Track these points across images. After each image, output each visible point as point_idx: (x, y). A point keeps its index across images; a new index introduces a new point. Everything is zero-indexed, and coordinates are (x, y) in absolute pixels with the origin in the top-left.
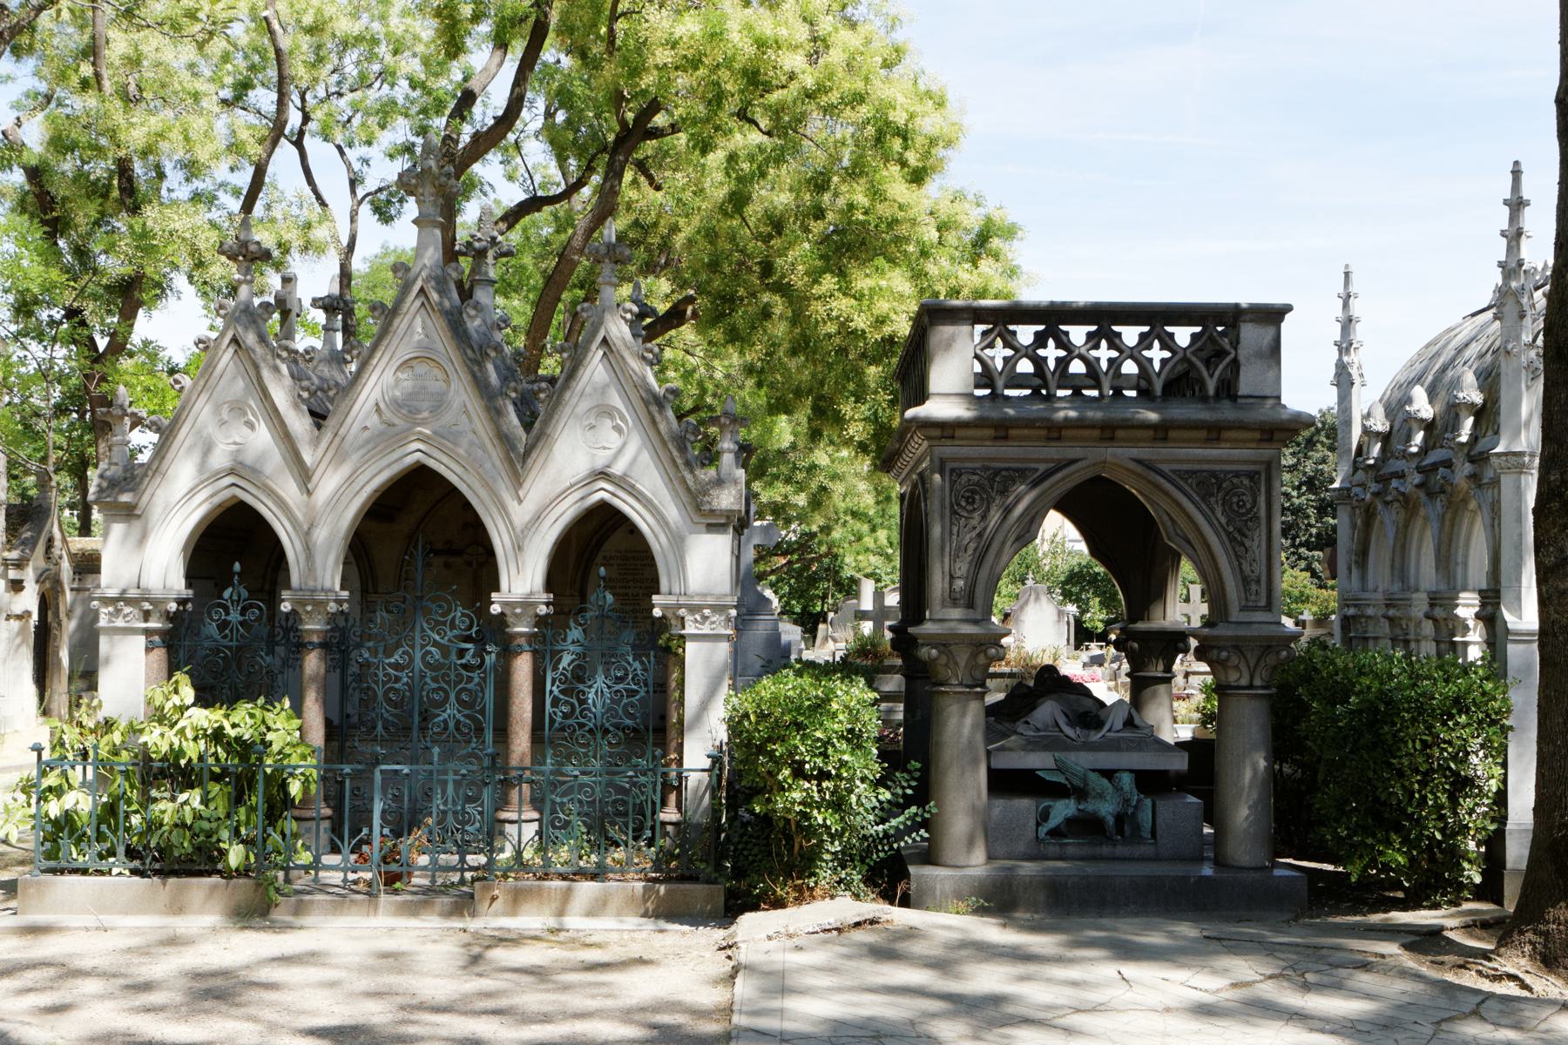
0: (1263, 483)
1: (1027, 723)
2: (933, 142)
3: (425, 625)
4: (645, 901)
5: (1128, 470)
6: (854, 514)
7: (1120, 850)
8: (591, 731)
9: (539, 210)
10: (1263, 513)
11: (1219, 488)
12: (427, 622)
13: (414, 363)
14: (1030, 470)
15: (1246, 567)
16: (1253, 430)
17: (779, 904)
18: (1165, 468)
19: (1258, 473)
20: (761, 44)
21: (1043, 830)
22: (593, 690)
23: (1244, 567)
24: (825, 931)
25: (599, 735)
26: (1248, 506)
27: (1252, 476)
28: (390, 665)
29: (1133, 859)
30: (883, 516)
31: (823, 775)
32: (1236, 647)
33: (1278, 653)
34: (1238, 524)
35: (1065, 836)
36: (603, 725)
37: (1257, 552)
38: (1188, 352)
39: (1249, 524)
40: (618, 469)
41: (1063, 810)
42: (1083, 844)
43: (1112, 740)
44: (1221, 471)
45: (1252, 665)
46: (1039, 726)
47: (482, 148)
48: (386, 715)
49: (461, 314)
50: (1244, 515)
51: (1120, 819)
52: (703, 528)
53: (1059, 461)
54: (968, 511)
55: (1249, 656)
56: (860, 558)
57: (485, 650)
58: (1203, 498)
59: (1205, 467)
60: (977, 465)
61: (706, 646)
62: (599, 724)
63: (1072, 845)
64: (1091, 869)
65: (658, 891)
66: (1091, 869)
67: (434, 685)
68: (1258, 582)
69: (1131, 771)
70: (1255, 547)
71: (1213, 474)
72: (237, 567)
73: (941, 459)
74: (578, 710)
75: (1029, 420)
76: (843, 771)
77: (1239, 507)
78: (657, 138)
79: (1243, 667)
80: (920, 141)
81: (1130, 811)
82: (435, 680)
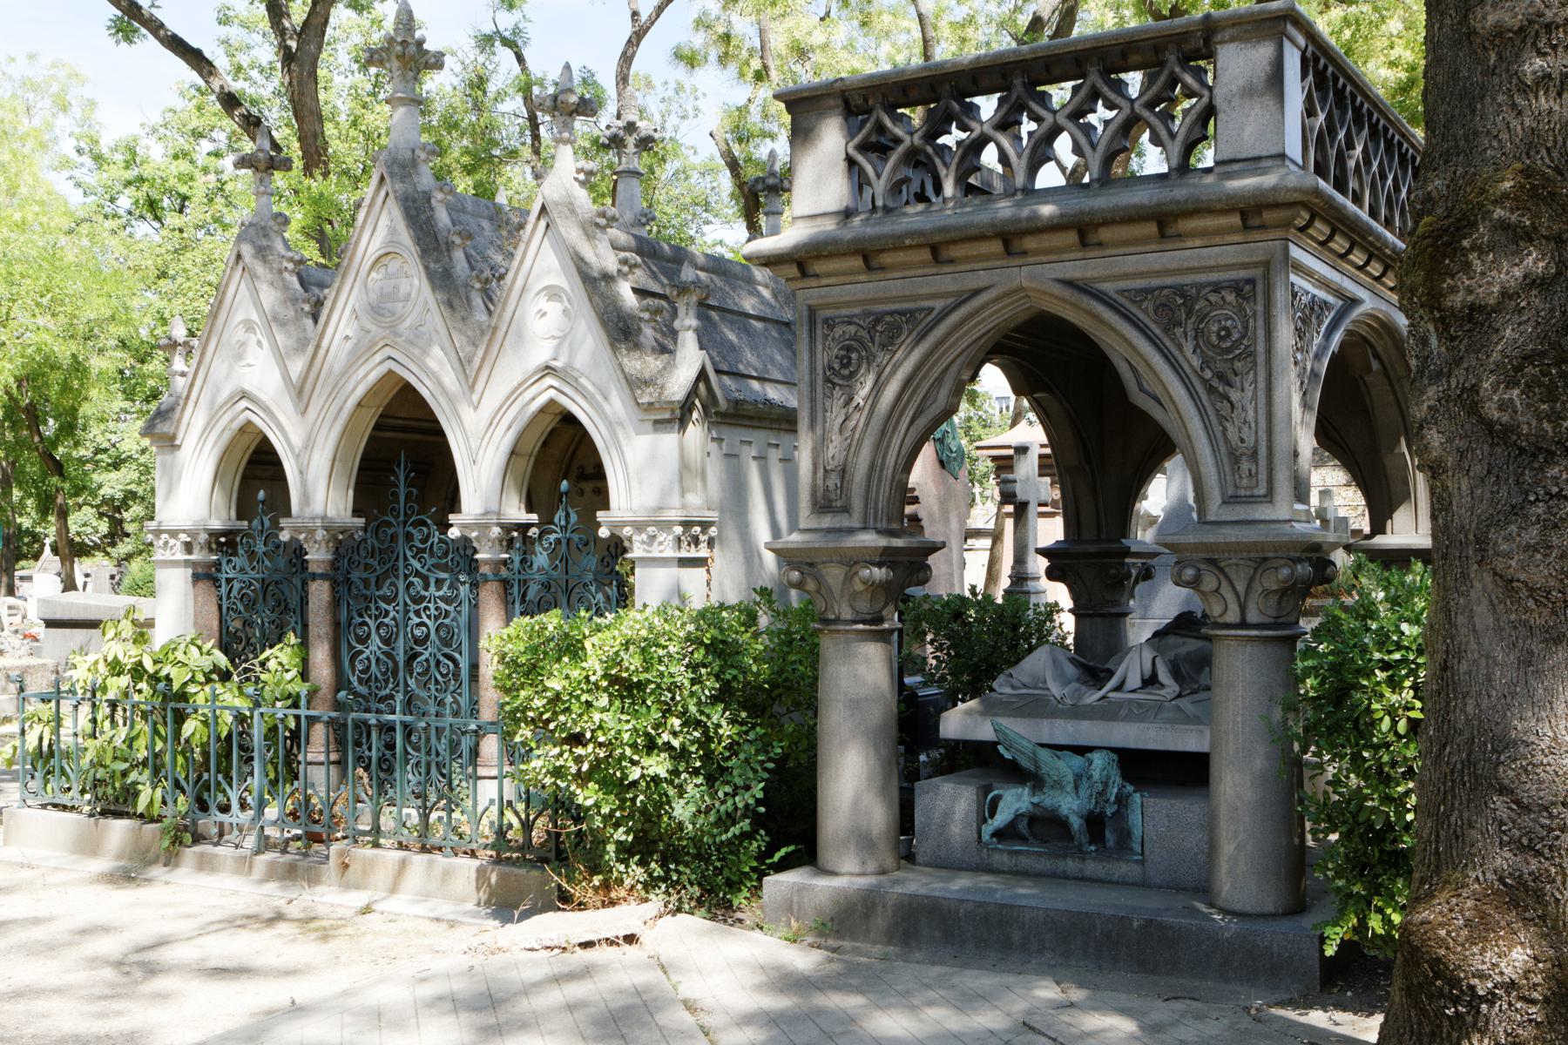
1: (1011, 675)
3: (409, 554)
7: (1092, 868)
10: (1261, 348)
11: (1189, 313)
12: (410, 548)
13: (385, 260)
14: (920, 310)
18: (1108, 287)
19: (1251, 282)
21: (987, 830)
23: (1230, 434)
26: (1236, 336)
27: (1236, 287)
28: (441, 598)
29: (1110, 882)
31: (577, 739)
32: (1212, 562)
34: (1220, 366)
35: (1022, 839)
38: (1137, 105)
39: (1238, 365)
41: (1014, 801)
43: (1120, 704)
44: (1191, 285)
45: (1241, 588)
46: (1025, 680)
48: (378, 653)
49: (429, 200)
50: (1229, 350)
51: (1095, 823)
52: (649, 426)
53: (958, 294)
54: (843, 378)
55: (1234, 577)
57: (458, 580)
58: (1166, 331)
59: (1169, 281)
60: (857, 310)
63: (1031, 856)
65: (489, 879)
67: (417, 620)
68: (1254, 455)
70: (1246, 402)
71: (1180, 290)
72: (261, 494)
73: (810, 307)
77: (1220, 338)
81: (1109, 811)
82: (417, 613)
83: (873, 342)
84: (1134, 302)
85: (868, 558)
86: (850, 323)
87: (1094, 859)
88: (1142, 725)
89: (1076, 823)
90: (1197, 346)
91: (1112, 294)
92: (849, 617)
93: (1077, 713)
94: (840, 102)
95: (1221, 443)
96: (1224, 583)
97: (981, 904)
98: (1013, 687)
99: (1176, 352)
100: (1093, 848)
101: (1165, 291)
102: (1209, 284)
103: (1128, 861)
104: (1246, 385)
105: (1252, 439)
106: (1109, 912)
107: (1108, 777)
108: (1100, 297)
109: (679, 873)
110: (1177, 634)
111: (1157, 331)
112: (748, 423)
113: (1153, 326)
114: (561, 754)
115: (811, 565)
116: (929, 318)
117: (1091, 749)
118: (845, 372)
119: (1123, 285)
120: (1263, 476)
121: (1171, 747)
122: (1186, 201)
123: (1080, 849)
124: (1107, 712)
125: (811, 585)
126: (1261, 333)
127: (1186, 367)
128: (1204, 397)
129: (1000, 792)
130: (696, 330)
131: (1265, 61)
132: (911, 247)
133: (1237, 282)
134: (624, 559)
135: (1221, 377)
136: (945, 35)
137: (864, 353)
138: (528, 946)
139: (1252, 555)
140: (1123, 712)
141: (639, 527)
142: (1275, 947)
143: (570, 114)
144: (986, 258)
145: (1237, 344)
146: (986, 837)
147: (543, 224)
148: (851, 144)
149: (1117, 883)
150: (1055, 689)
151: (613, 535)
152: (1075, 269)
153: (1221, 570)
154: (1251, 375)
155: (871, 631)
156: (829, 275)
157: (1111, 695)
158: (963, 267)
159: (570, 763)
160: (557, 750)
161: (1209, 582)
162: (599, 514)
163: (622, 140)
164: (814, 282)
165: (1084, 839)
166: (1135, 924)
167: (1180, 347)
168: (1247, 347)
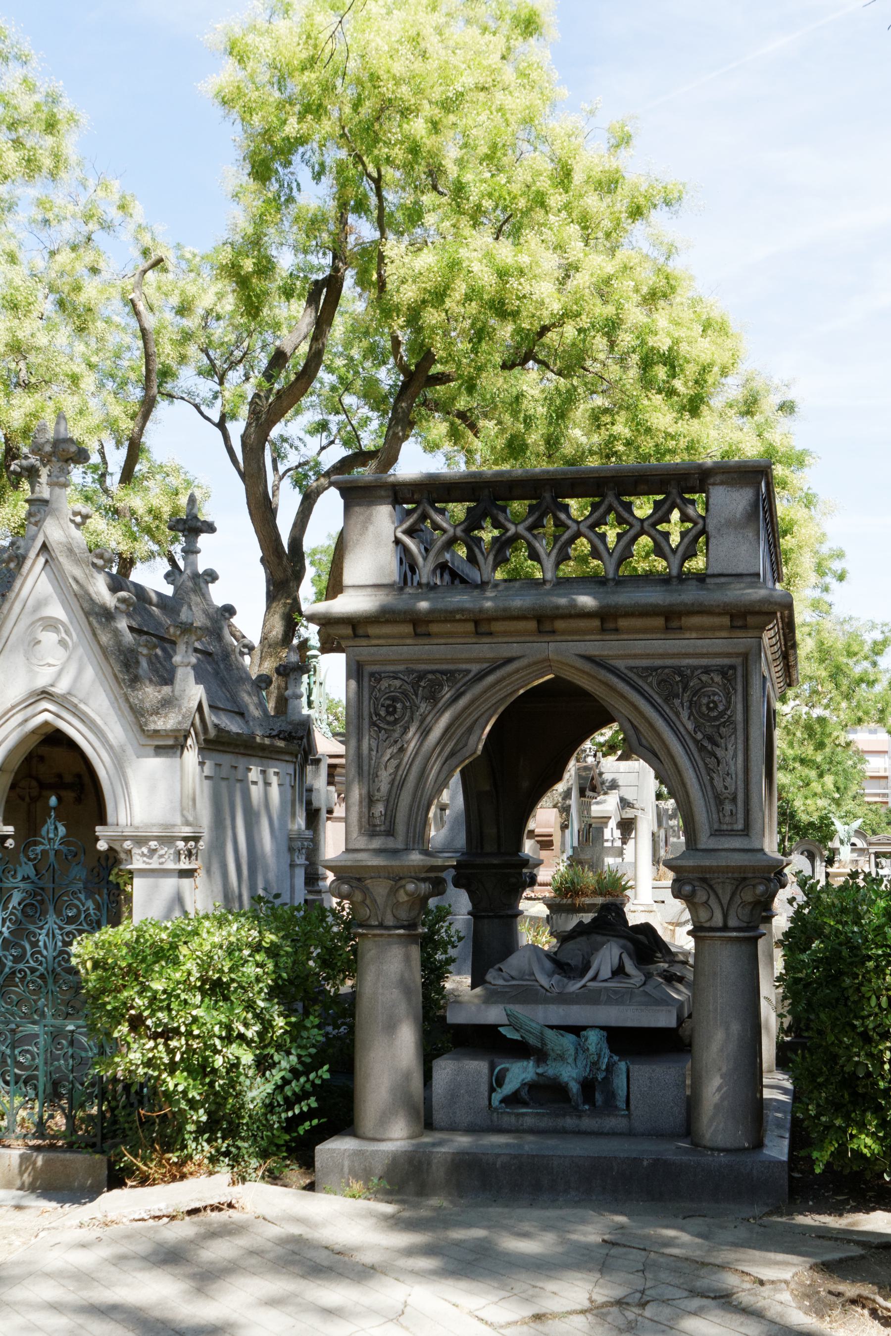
0: (739, 680)
1: (501, 970)
2: (705, 369)
4: (21, 1173)
5: (577, 669)
6: (803, 761)
7: (587, 1123)
8: (42, 976)
9: (364, 465)
10: (739, 717)
11: (685, 689)
14: (460, 671)
15: (718, 783)
16: (719, 614)
17: (144, 1181)
18: (620, 664)
19: (733, 667)
20: (502, 274)
21: (497, 1097)
22: (44, 931)
23: (716, 782)
24: (155, 1217)
25: (50, 981)
27: (723, 671)
30: (831, 762)
31: (168, 1033)
32: (704, 880)
33: (754, 886)
34: (709, 730)
35: (525, 1104)
36: (54, 970)
37: (732, 763)
38: (646, 524)
39: (723, 730)
40: (60, 689)
42: (543, 1115)
43: (599, 991)
44: (688, 667)
45: (725, 901)
46: (513, 973)
47: (285, 404)
50: (716, 719)
51: (588, 1086)
54: (388, 723)
55: (720, 892)
56: (809, 802)
58: (666, 700)
59: (669, 662)
60: (401, 668)
61: (150, 881)
62: (50, 969)
63: (529, 1116)
64: (530, 1144)
65: (35, 1163)
66: (530, 1144)
68: (734, 800)
69: (602, 1028)
71: (678, 670)
74: (29, 954)
75: (446, 611)
76: (194, 1027)
78: (444, 383)
79: (713, 902)
80: (691, 370)
81: (600, 1077)
83: (416, 695)
84: (640, 677)
85: (413, 874)
86: (396, 678)
88: (622, 1008)
89: (574, 1087)
91: (623, 669)
92: (391, 924)
93: (563, 999)
94: (390, 493)
95: (709, 788)
96: (712, 897)
97: (515, 1157)
98: (505, 980)
99: (674, 718)
100: (587, 1107)
101: (666, 671)
102: (701, 667)
103: (617, 1116)
104: (729, 746)
105: (733, 787)
106: (622, 1155)
107: (601, 1050)
108: (613, 671)
109: (238, 1148)
110: (598, 933)
111: (659, 701)
112: (221, 748)
113: (656, 697)
114: (156, 1047)
115: (359, 880)
117: (584, 1028)
119: (632, 663)
121: (629, 1024)
122: (693, 604)
123: (576, 1108)
124: (590, 998)
125: (358, 897)
126: (740, 707)
127: (682, 730)
129: (507, 1065)
130: (194, 667)
132: (460, 621)
133: (723, 667)
134: (121, 870)
135: (710, 739)
136: (166, 351)
137: (408, 704)
138: (137, 1217)
139: (736, 875)
140: (603, 998)
141: (140, 841)
142: (755, 1172)
143: (66, 461)
145: (722, 714)
146: (495, 1102)
147: (42, 560)
148: (399, 529)
150: (543, 980)
151: (111, 849)
152: (593, 648)
153: (711, 887)
154: (733, 737)
155: (737, 937)
156: (379, 637)
157: (589, 984)
158: (500, 640)
159: (164, 1055)
160: (151, 1044)
161: (701, 896)
162: (98, 828)
163: (38, 470)
164: (364, 642)
165: (580, 1101)
166: (645, 1163)
167: (677, 714)
168: (730, 717)
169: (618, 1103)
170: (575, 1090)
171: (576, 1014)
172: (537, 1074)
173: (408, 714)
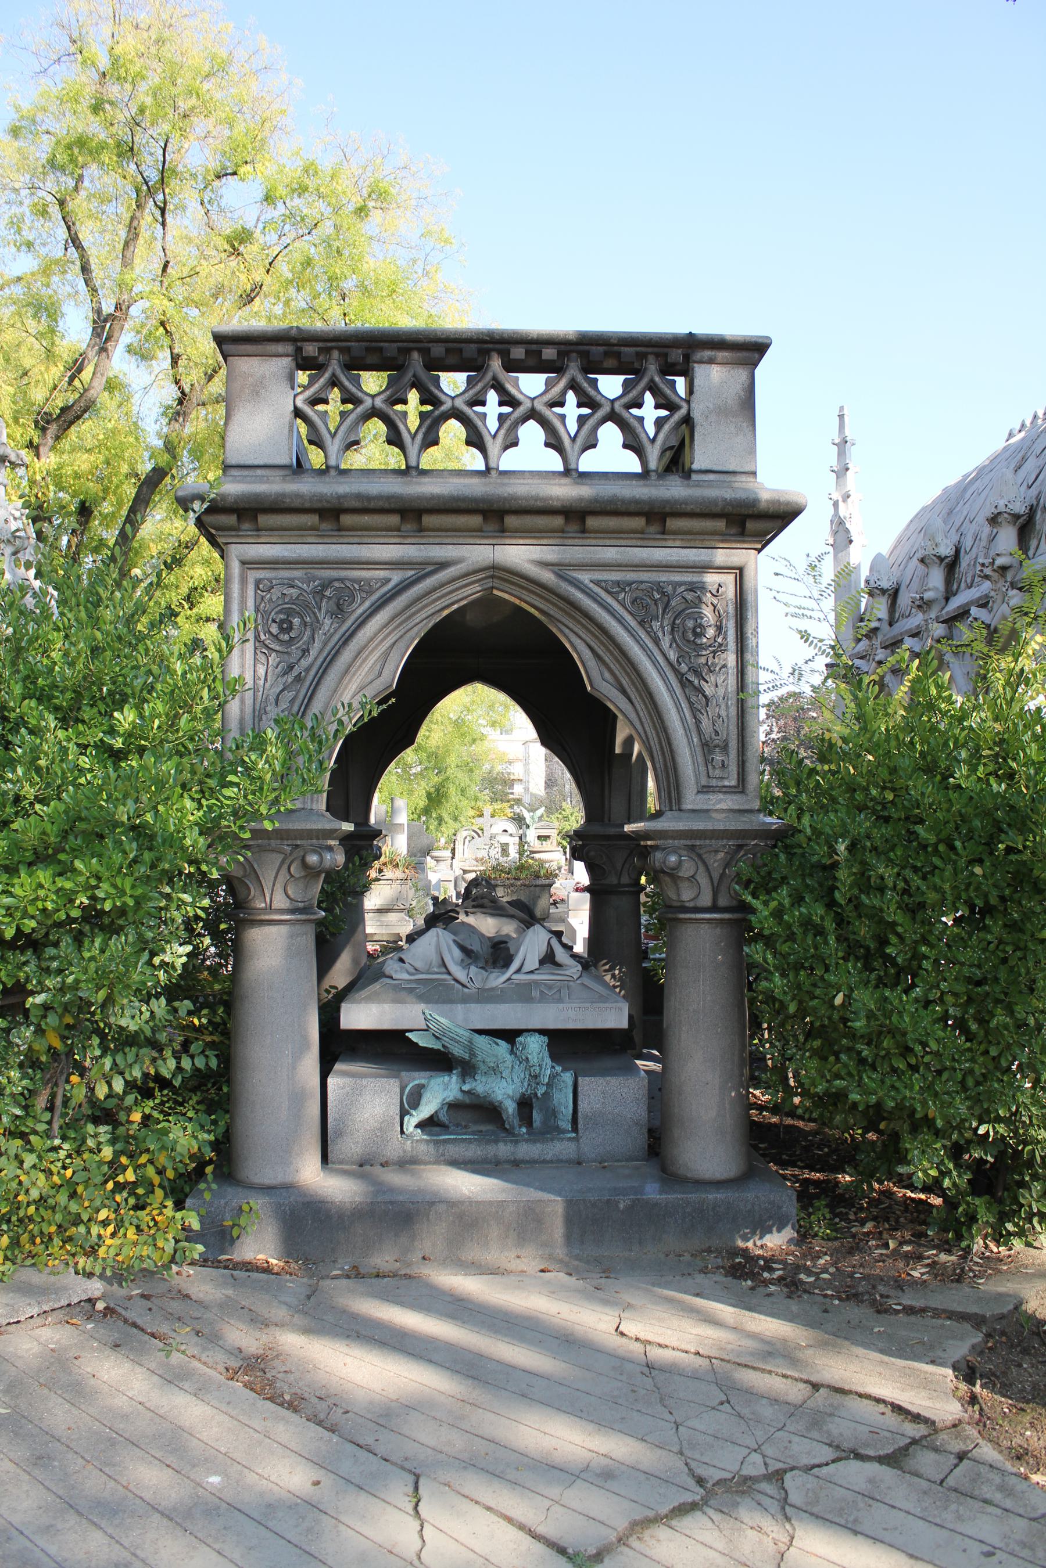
7: (526, 1150)
44: (669, 583)
46: (419, 965)
51: (525, 1104)
58: (641, 623)
59: (644, 576)
68: (725, 748)
69: (542, 1032)
71: (659, 587)
87: (527, 1141)
90: (674, 640)
91: (587, 582)
93: (485, 996)
96: (702, 869)
103: (562, 1139)
105: (725, 732)
116: (385, 589)
117: (519, 1032)
118: (286, 637)
120: (733, 769)
123: (509, 1132)
124: (524, 994)
128: (678, 690)
131: (739, 387)
144: (714, 533)
149: (552, 1162)
153: (700, 856)
155: (721, 920)
157: (515, 977)
165: (516, 1122)
166: (621, 1206)
167: (657, 642)
169: (560, 1123)
170: (510, 1111)
171: (506, 1017)
172: (462, 1091)
173: (308, 632)
